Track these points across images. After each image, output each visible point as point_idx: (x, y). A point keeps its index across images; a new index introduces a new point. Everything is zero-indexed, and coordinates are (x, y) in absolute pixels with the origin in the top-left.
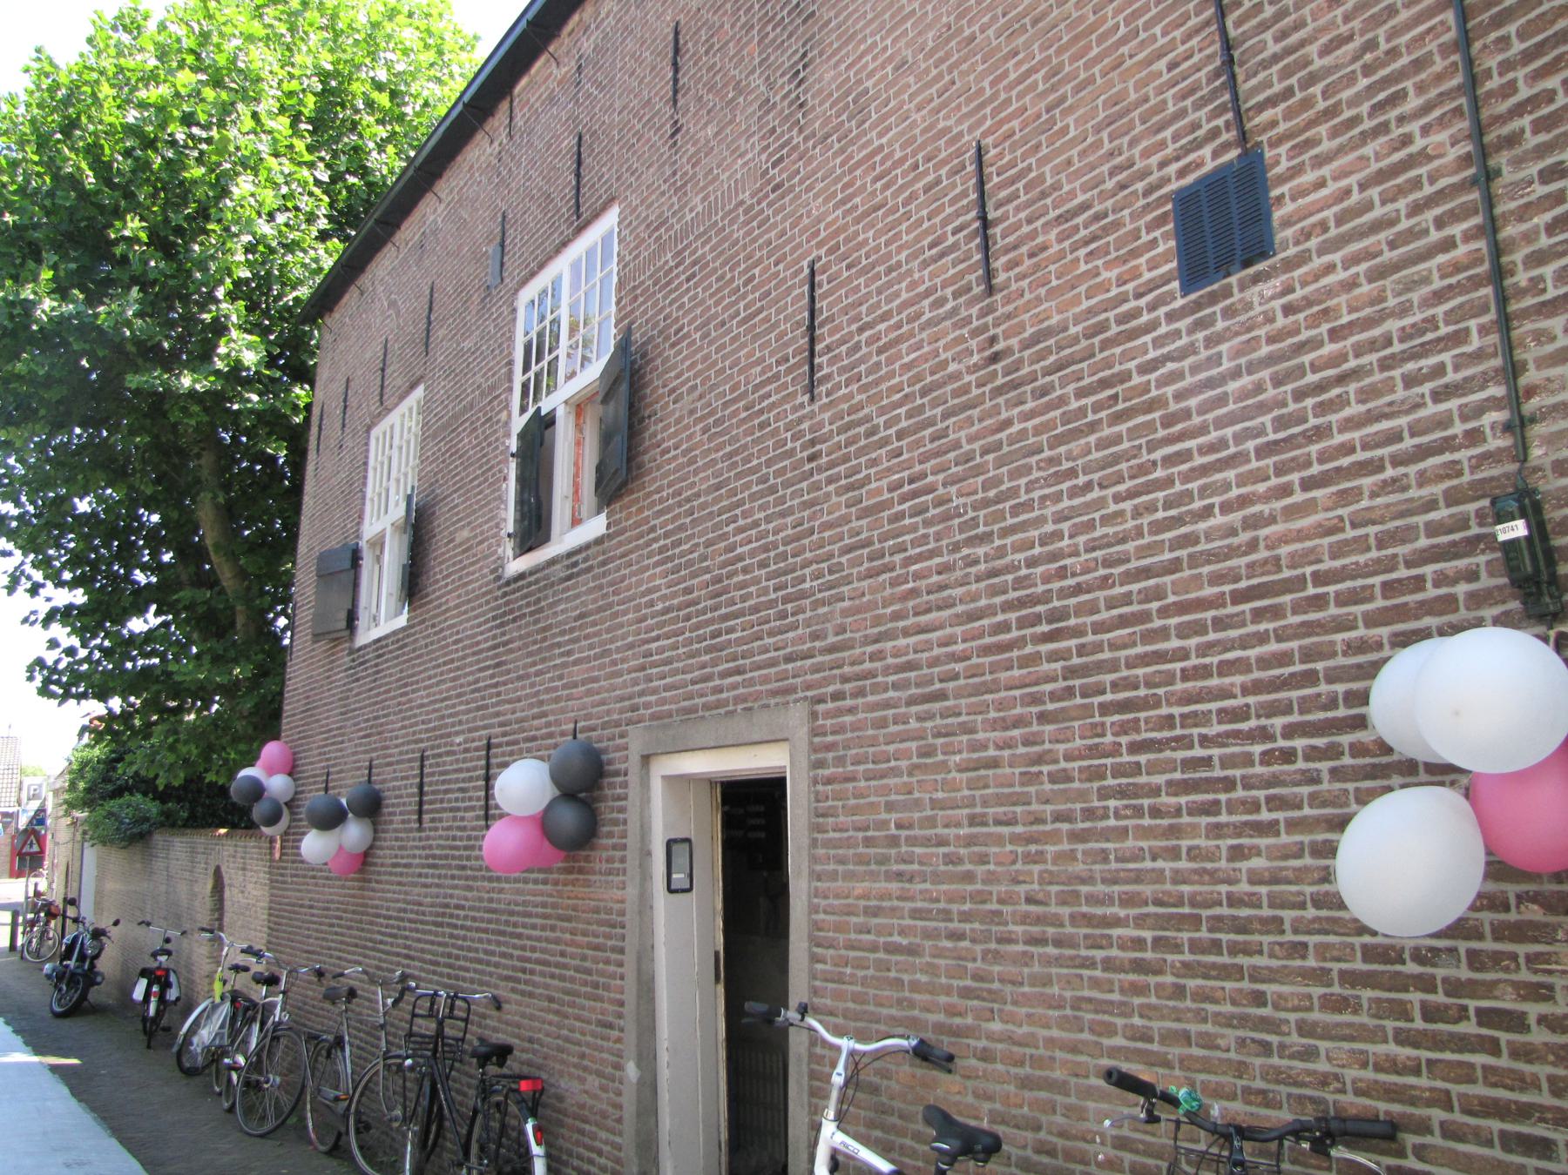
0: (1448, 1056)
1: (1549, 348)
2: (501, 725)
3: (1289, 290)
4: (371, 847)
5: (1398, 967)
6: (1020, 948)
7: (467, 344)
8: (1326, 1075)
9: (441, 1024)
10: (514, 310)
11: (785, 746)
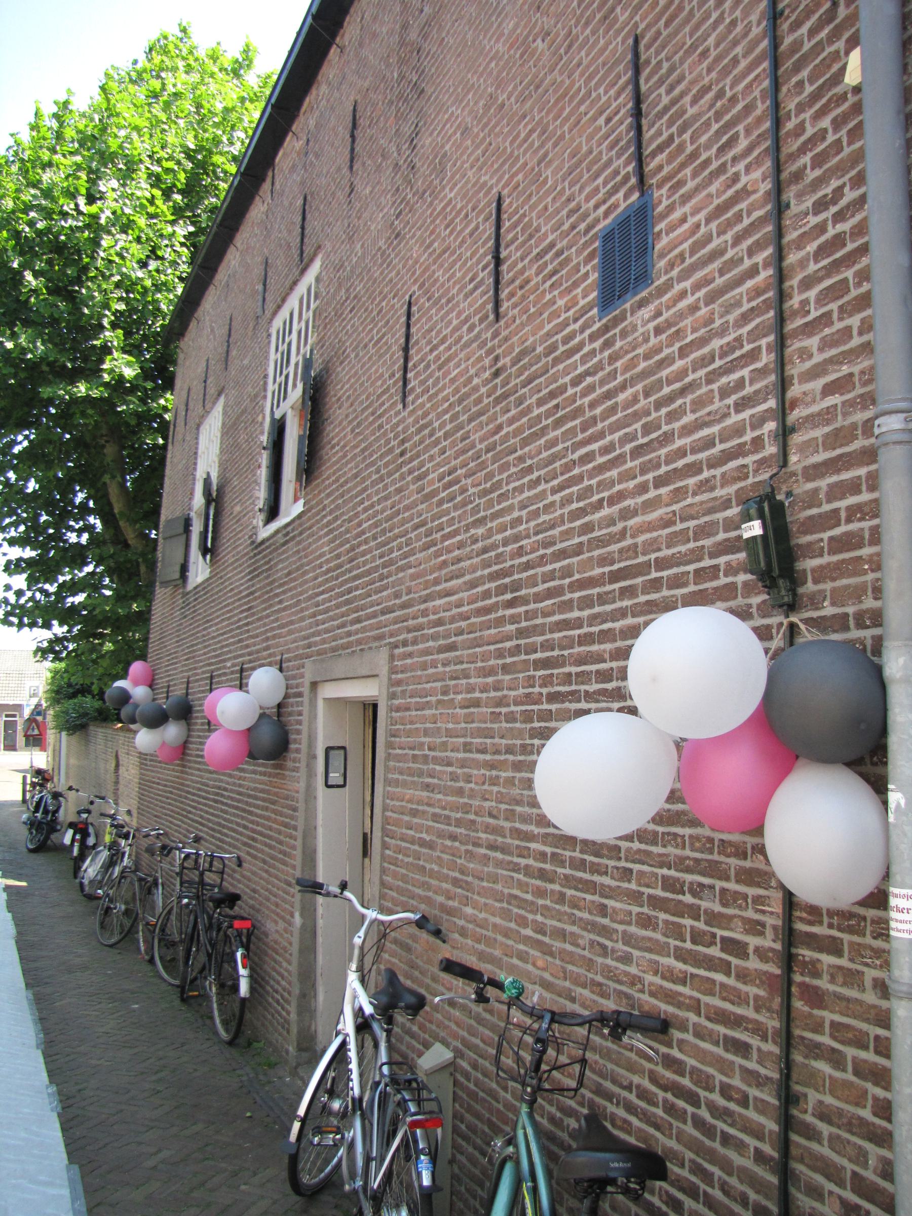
0: (702, 972)
1: (808, 365)
2: (249, 654)
3: (658, 314)
4: (186, 742)
5: (680, 897)
6: (483, 851)
7: (246, 362)
8: (634, 976)
9: (202, 874)
10: (269, 335)
11: (376, 680)
